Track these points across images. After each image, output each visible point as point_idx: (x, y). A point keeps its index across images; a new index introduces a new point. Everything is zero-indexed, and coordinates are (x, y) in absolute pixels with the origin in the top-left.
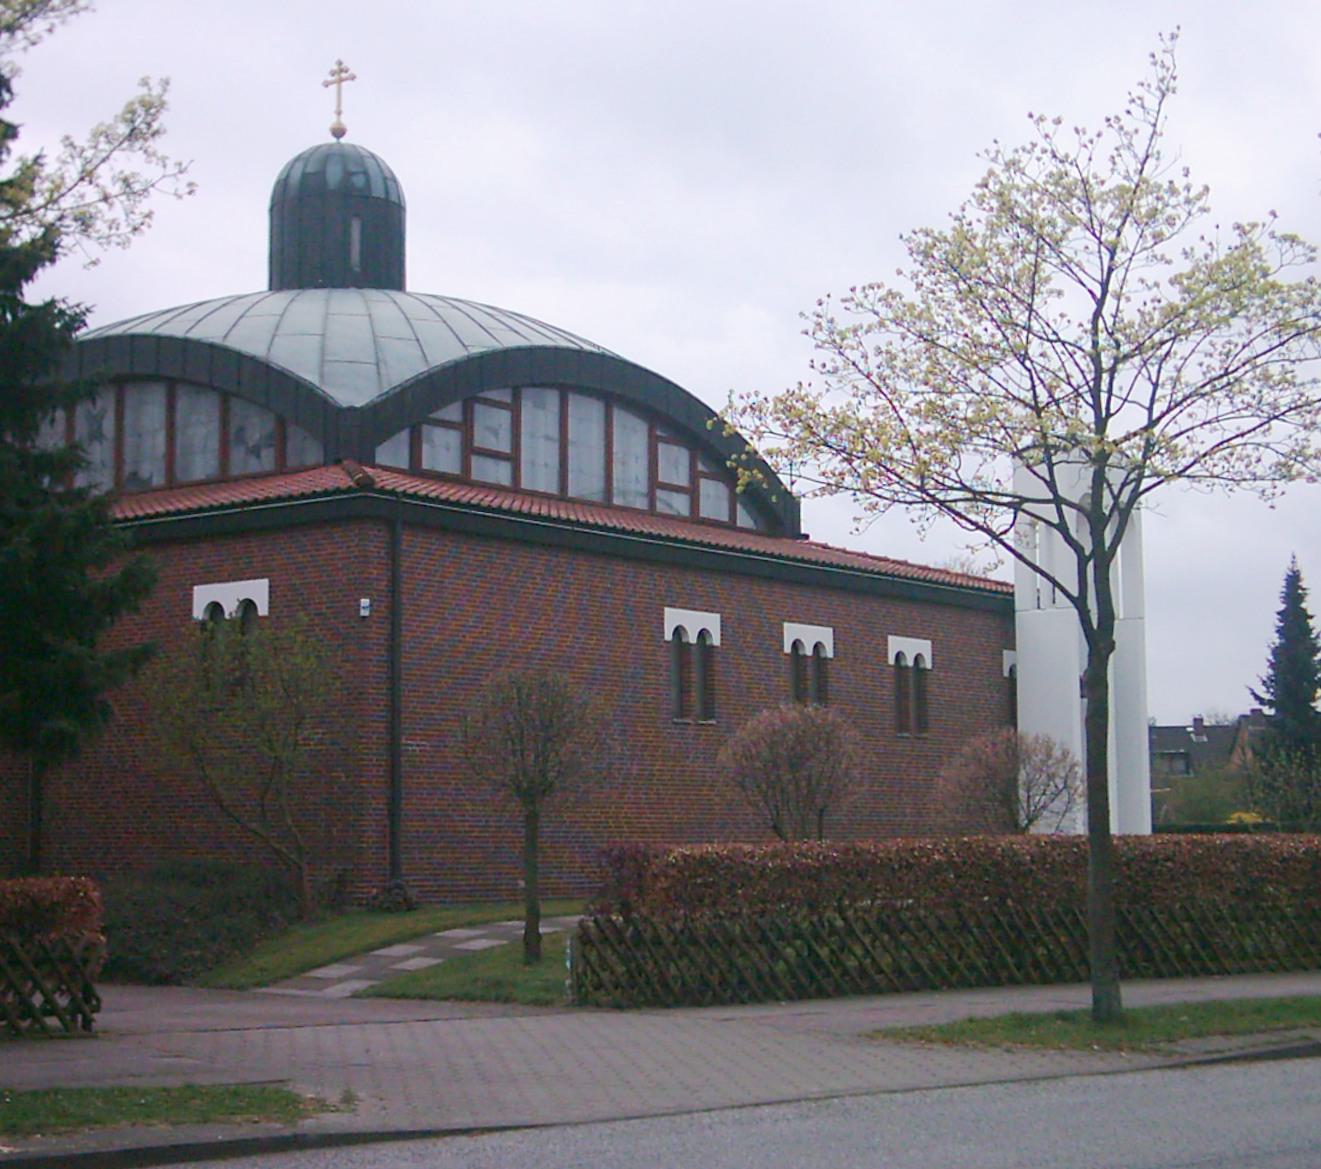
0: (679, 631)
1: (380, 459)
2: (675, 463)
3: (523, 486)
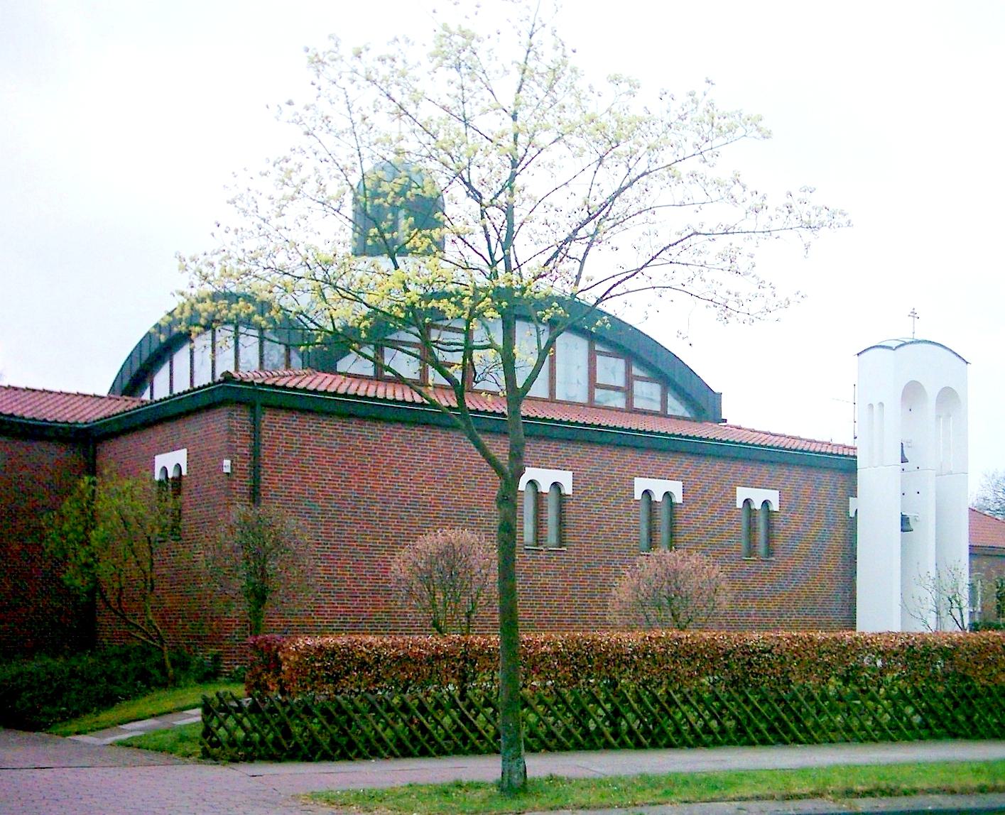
0: (747, 502)
2: (612, 370)
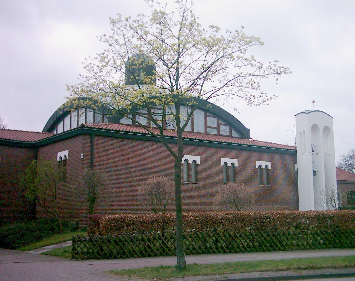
0: (260, 166)
1: (120, 122)
2: (213, 122)
3: (194, 131)
